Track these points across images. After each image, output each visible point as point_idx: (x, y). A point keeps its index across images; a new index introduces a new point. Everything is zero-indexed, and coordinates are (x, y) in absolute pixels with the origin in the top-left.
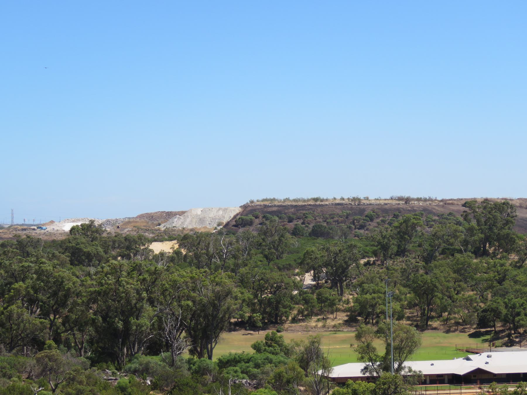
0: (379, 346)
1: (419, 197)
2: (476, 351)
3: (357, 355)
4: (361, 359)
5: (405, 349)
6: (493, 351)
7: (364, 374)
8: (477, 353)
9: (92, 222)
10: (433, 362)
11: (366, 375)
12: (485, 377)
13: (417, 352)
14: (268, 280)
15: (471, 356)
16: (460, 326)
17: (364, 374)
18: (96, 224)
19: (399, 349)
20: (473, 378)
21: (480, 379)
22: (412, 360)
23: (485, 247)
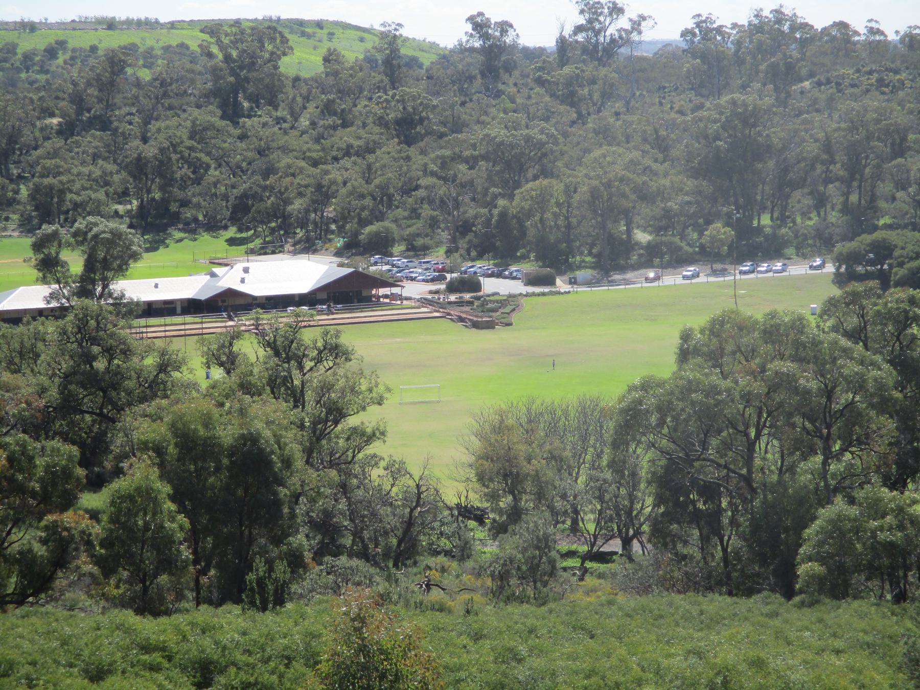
0: (75, 262)
1: (152, 16)
2: (225, 261)
3: (35, 274)
4: (44, 281)
5: (107, 261)
6: (252, 261)
7: (48, 302)
8: (226, 265)
9: (46, 19)
10: (157, 280)
11: (51, 306)
12: (241, 301)
13: (135, 267)
14: (753, 351)
15: (217, 270)
16: (213, 226)
17: (48, 302)
18: (766, 13)
19: (106, 265)
20: (220, 304)
21: (232, 306)
22: (125, 277)
23: (236, 97)
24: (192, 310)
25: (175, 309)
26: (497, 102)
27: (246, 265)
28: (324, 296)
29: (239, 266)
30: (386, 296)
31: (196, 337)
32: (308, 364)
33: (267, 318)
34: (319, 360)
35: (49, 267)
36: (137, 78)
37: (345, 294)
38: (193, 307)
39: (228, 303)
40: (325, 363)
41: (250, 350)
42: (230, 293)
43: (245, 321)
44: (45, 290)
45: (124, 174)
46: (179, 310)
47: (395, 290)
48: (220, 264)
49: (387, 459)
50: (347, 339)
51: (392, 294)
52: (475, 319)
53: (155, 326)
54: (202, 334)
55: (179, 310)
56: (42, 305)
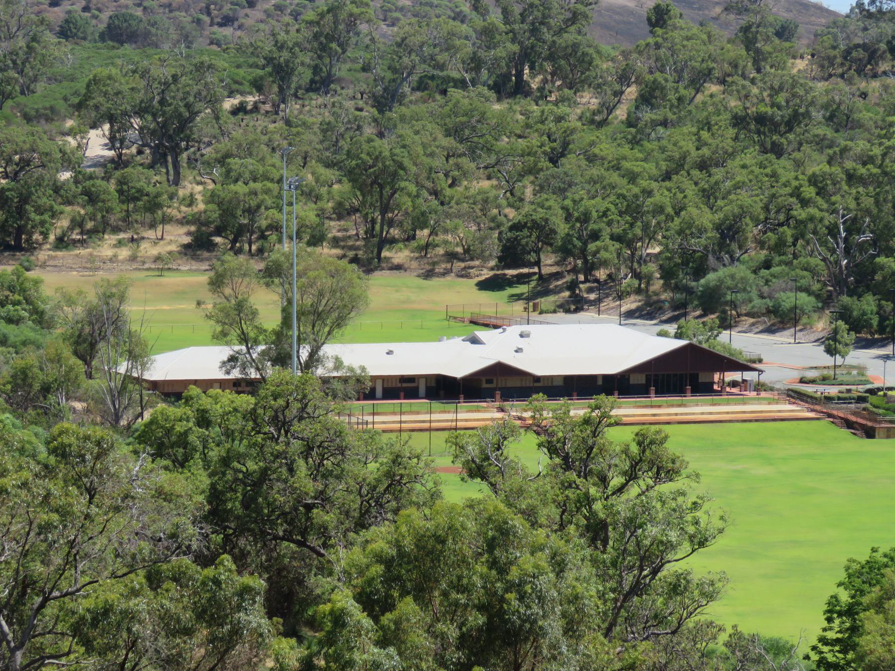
0: (267, 307)
2: (494, 321)
6: (534, 323)
23: (520, 74)
24: (442, 393)
25: (417, 389)
26: (77, 548)
27: (525, 328)
28: (640, 379)
29: (514, 331)
30: (734, 384)
31: (446, 434)
32: (616, 481)
33: (549, 410)
34: (631, 476)
35: (233, 321)
36: (320, 378)
37: (682, 374)
38: (443, 389)
39: (499, 383)
40: (641, 482)
41: (528, 456)
42: (500, 370)
43: (519, 410)
44: (223, 352)
45: (346, 186)
46: (422, 390)
47: (749, 376)
48: (487, 325)
49: (730, 631)
50: (677, 443)
51: (744, 381)
52: (869, 424)
53: (387, 417)
54: (456, 429)
55: (422, 390)
56: (220, 375)
